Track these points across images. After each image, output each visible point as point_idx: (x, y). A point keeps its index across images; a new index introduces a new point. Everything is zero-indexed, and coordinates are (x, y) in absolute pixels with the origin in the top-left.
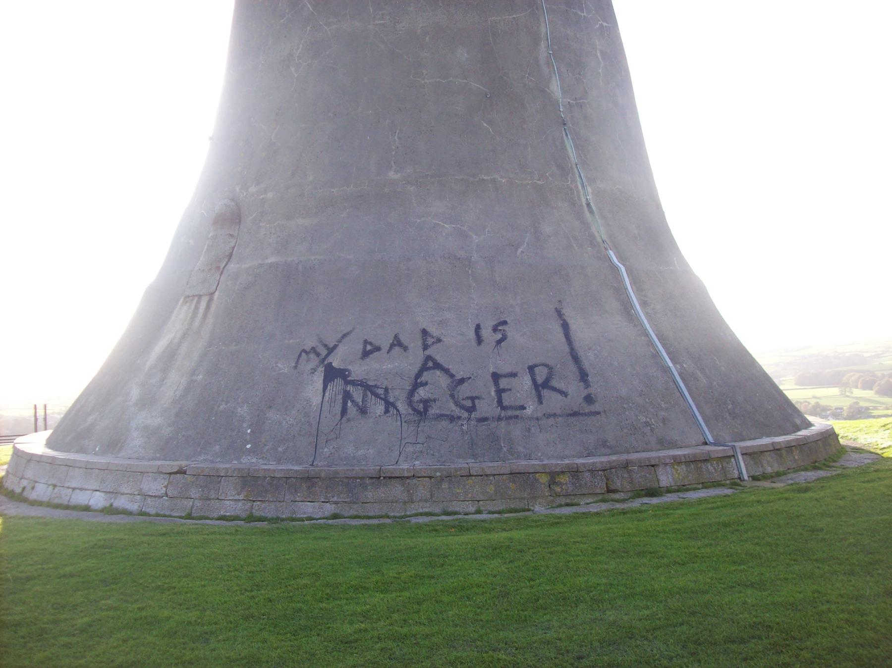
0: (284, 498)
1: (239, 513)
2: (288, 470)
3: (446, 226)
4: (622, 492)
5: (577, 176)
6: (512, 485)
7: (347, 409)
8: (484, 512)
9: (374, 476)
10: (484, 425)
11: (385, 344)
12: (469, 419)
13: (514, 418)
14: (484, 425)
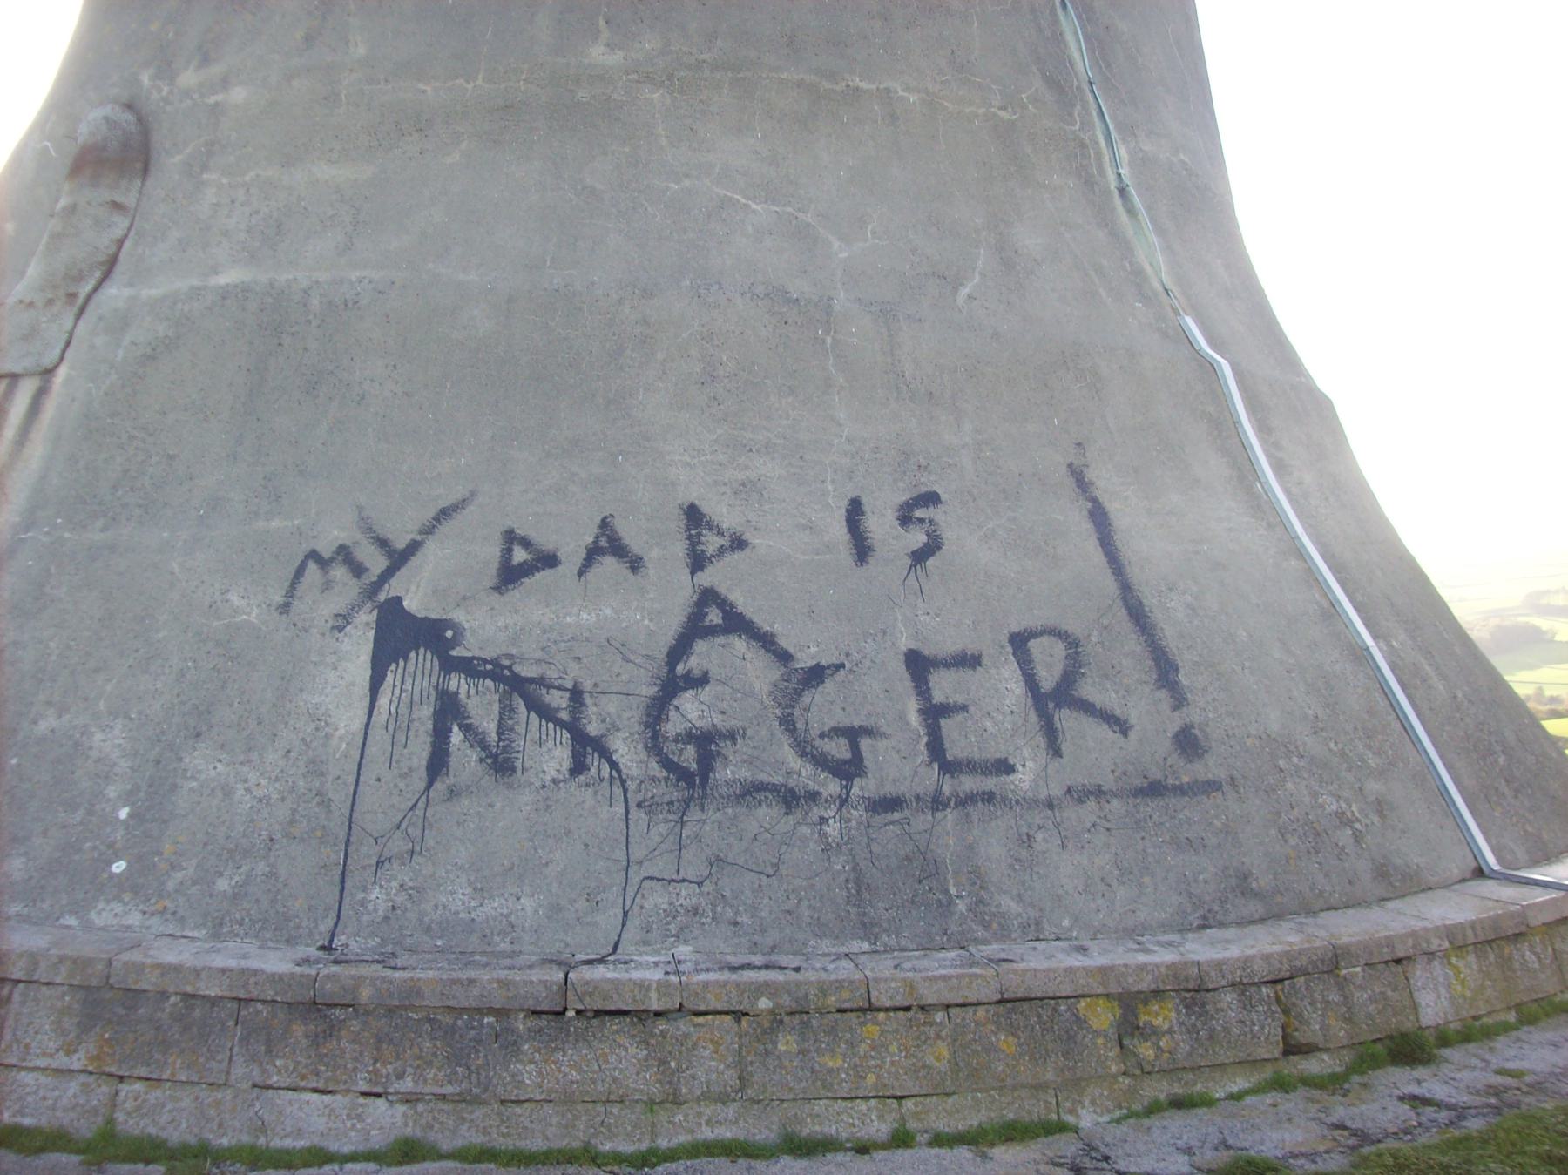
0: (228, 1073)
1: (65, 1122)
2: (243, 971)
3: (754, 206)
4: (1326, 1050)
5: (1094, 113)
6: (1006, 1042)
7: (447, 753)
8: (919, 1138)
9: (544, 1007)
10: (892, 823)
11: (572, 550)
12: (843, 801)
13: (983, 801)
14: (892, 823)
